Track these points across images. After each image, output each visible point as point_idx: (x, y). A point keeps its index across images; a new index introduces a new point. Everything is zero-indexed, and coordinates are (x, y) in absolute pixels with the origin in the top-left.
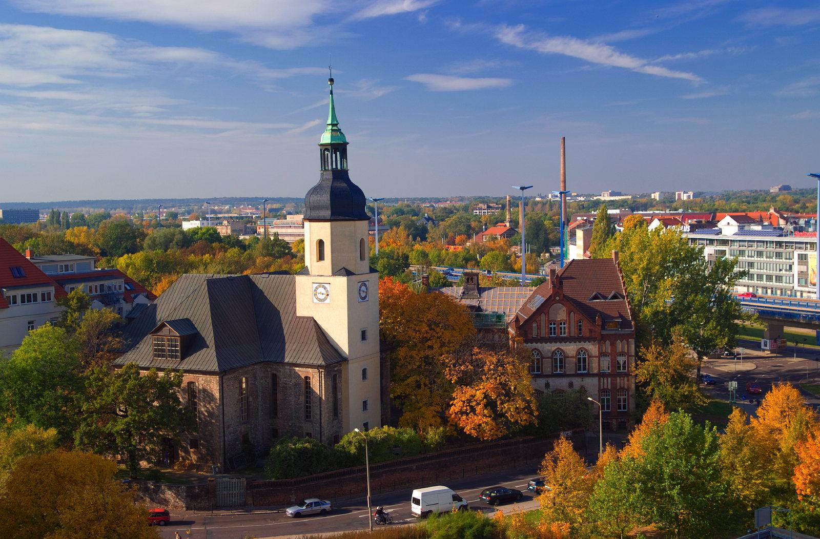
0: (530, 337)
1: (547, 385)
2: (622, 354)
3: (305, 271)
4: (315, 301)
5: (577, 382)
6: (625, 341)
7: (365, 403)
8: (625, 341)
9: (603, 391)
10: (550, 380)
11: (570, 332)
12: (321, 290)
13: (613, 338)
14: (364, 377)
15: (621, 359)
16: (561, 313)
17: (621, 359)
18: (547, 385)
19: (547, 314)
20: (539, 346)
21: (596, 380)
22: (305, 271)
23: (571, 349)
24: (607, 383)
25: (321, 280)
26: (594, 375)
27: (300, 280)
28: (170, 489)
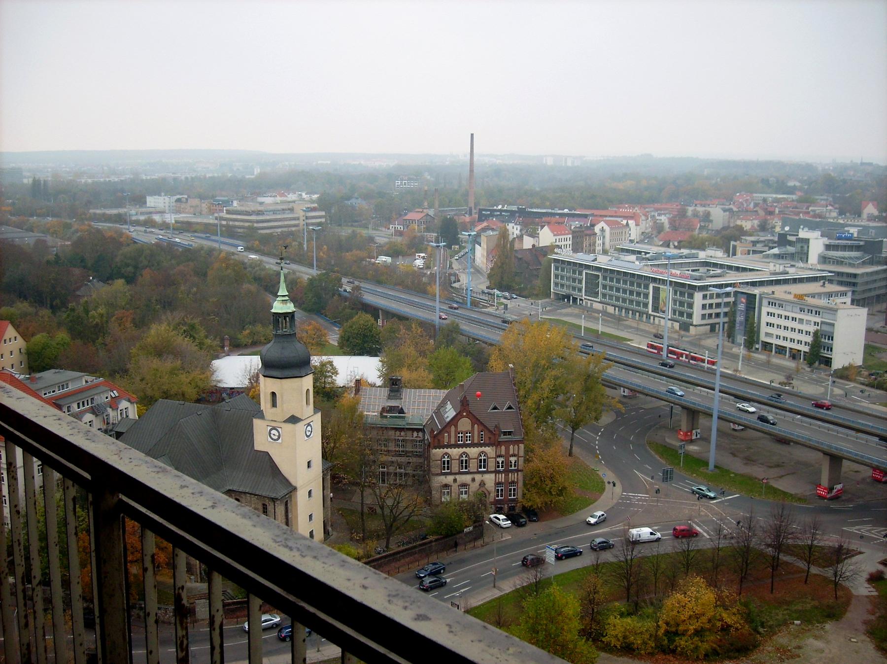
0: (442, 444)
1: (455, 480)
2: (513, 455)
3: (261, 415)
4: (270, 439)
5: (478, 477)
6: (516, 446)
7: (311, 516)
8: (516, 446)
9: (498, 484)
10: (457, 477)
11: (415, 393)
12: (273, 432)
13: (507, 443)
14: (309, 466)
15: (513, 459)
16: (465, 424)
17: (513, 459)
18: (455, 480)
19: (456, 426)
20: (449, 450)
21: (493, 476)
22: (261, 415)
23: (473, 452)
24: (502, 478)
25: (274, 424)
26: (491, 472)
27: (257, 422)
28: (318, 275)
